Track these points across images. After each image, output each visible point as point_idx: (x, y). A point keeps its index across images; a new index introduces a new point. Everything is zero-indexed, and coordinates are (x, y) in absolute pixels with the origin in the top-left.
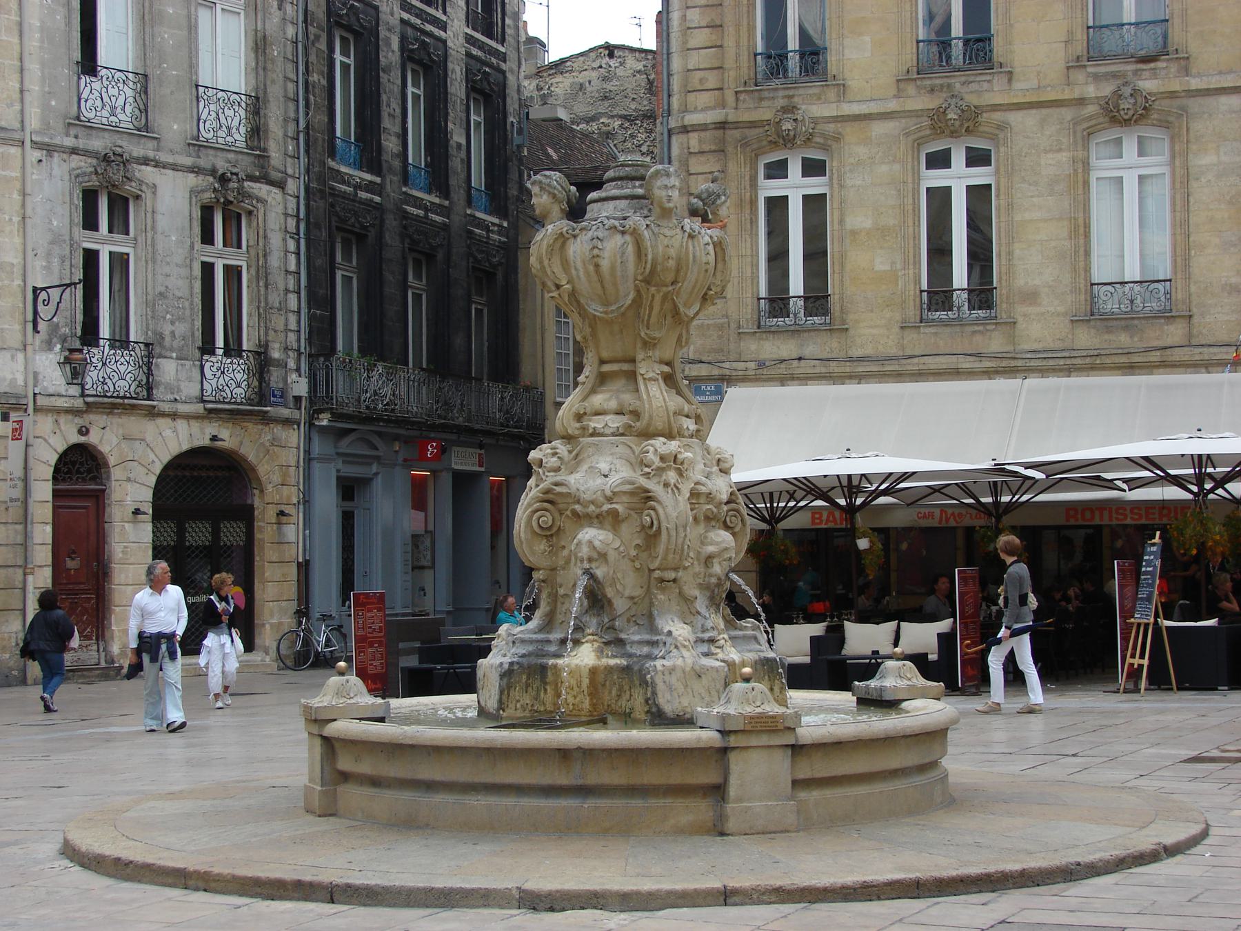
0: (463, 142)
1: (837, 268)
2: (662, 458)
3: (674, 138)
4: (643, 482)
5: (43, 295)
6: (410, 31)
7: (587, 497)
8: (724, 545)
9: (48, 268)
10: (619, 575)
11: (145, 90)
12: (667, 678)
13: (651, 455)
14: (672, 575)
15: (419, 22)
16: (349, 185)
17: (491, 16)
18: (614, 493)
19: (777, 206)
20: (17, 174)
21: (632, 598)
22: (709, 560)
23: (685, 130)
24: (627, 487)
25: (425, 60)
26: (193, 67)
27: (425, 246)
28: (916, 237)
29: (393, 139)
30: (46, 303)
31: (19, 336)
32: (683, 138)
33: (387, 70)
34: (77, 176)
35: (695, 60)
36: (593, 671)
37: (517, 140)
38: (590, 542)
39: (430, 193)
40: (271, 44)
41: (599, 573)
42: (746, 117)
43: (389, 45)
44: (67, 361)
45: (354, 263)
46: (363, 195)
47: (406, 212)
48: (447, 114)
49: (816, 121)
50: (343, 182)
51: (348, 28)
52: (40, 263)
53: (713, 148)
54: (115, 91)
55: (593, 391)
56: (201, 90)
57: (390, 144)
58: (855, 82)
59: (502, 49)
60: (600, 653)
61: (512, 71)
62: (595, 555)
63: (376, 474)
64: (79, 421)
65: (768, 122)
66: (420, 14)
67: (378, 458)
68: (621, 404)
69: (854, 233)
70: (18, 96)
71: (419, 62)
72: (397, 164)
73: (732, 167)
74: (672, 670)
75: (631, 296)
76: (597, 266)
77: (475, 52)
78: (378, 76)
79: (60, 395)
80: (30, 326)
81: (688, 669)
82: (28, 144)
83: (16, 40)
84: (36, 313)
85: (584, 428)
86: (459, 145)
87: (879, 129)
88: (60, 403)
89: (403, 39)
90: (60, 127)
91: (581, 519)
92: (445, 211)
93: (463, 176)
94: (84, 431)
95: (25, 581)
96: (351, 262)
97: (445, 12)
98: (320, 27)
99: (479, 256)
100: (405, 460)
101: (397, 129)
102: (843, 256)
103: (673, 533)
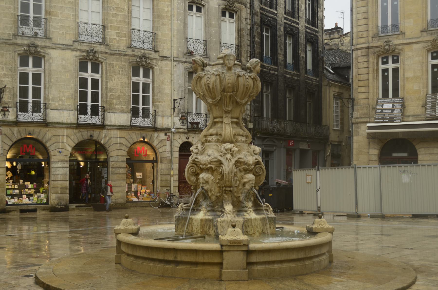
0: (304, 56)
1: (402, 89)
2: (226, 150)
3: (354, 52)
4: (220, 158)
5: (176, 101)
6: (287, 26)
7: (203, 162)
8: (250, 179)
9: (178, 94)
10: (213, 189)
11: (206, 45)
12: (222, 224)
13: (222, 149)
14: (229, 189)
15: (290, 23)
16: (267, 69)
17: (314, 20)
18: (211, 162)
19: (385, 71)
20: (169, 69)
21: (217, 196)
22: (244, 184)
23: (357, 49)
24: (215, 160)
25: (292, 33)
26: (220, 38)
27: (291, 86)
28: (427, 79)
29: (282, 56)
30: (177, 103)
31: (170, 113)
32: (356, 52)
33: (280, 37)
34: (186, 69)
35: (360, 29)
36: (202, 220)
37: (322, 55)
38: (203, 178)
39: (293, 71)
40: (243, 30)
41: (205, 188)
42: (375, 45)
43: (280, 29)
44: (181, 119)
45: (270, 91)
46: (271, 72)
47: (285, 76)
48: (299, 48)
49: (396, 45)
50: (265, 68)
51: (268, 25)
52: (176, 93)
53: (365, 54)
54: (197, 45)
55: (211, 128)
56: (222, 44)
57: (281, 57)
58: (408, 33)
59: (317, 30)
60: (205, 214)
61: (320, 36)
62: (204, 182)
63: (275, 150)
64: (186, 135)
65: (381, 46)
66: (290, 21)
67: (276, 145)
68: (217, 132)
69: (407, 78)
70: (170, 48)
71: (290, 34)
72: (283, 63)
73: (371, 60)
74: (223, 221)
75: (220, 96)
76: (209, 87)
77: (308, 31)
78: (277, 39)
79: (181, 129)
80: (173, 110)
81: (229, 221)
82: (173, 60)
83: (170, 33)
84: (174, 106)
85: (206, 140)
86: (303, 57)
87: (415, 46)
88: (181, 131)
89: (285, 28)
90: (182, 56)
91: (202, 170)
92: (298, 76)
93: (304, 66)
94: (188, 138)
95: (171, 179)
96: (269, 90)
97: (298, 20)
98: (258, 25)
99: (309, 88)
100: (284, 146)
101: (283, 53)
102: (404, 85)
103: (227, 175)
